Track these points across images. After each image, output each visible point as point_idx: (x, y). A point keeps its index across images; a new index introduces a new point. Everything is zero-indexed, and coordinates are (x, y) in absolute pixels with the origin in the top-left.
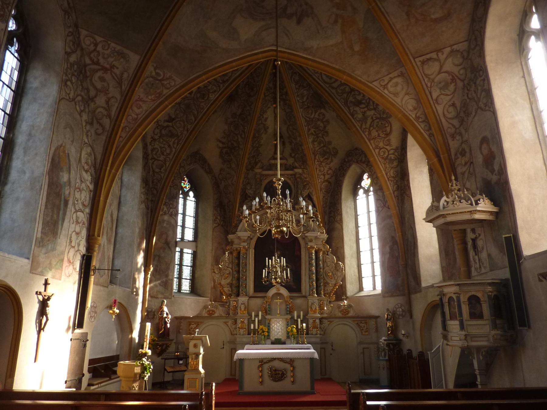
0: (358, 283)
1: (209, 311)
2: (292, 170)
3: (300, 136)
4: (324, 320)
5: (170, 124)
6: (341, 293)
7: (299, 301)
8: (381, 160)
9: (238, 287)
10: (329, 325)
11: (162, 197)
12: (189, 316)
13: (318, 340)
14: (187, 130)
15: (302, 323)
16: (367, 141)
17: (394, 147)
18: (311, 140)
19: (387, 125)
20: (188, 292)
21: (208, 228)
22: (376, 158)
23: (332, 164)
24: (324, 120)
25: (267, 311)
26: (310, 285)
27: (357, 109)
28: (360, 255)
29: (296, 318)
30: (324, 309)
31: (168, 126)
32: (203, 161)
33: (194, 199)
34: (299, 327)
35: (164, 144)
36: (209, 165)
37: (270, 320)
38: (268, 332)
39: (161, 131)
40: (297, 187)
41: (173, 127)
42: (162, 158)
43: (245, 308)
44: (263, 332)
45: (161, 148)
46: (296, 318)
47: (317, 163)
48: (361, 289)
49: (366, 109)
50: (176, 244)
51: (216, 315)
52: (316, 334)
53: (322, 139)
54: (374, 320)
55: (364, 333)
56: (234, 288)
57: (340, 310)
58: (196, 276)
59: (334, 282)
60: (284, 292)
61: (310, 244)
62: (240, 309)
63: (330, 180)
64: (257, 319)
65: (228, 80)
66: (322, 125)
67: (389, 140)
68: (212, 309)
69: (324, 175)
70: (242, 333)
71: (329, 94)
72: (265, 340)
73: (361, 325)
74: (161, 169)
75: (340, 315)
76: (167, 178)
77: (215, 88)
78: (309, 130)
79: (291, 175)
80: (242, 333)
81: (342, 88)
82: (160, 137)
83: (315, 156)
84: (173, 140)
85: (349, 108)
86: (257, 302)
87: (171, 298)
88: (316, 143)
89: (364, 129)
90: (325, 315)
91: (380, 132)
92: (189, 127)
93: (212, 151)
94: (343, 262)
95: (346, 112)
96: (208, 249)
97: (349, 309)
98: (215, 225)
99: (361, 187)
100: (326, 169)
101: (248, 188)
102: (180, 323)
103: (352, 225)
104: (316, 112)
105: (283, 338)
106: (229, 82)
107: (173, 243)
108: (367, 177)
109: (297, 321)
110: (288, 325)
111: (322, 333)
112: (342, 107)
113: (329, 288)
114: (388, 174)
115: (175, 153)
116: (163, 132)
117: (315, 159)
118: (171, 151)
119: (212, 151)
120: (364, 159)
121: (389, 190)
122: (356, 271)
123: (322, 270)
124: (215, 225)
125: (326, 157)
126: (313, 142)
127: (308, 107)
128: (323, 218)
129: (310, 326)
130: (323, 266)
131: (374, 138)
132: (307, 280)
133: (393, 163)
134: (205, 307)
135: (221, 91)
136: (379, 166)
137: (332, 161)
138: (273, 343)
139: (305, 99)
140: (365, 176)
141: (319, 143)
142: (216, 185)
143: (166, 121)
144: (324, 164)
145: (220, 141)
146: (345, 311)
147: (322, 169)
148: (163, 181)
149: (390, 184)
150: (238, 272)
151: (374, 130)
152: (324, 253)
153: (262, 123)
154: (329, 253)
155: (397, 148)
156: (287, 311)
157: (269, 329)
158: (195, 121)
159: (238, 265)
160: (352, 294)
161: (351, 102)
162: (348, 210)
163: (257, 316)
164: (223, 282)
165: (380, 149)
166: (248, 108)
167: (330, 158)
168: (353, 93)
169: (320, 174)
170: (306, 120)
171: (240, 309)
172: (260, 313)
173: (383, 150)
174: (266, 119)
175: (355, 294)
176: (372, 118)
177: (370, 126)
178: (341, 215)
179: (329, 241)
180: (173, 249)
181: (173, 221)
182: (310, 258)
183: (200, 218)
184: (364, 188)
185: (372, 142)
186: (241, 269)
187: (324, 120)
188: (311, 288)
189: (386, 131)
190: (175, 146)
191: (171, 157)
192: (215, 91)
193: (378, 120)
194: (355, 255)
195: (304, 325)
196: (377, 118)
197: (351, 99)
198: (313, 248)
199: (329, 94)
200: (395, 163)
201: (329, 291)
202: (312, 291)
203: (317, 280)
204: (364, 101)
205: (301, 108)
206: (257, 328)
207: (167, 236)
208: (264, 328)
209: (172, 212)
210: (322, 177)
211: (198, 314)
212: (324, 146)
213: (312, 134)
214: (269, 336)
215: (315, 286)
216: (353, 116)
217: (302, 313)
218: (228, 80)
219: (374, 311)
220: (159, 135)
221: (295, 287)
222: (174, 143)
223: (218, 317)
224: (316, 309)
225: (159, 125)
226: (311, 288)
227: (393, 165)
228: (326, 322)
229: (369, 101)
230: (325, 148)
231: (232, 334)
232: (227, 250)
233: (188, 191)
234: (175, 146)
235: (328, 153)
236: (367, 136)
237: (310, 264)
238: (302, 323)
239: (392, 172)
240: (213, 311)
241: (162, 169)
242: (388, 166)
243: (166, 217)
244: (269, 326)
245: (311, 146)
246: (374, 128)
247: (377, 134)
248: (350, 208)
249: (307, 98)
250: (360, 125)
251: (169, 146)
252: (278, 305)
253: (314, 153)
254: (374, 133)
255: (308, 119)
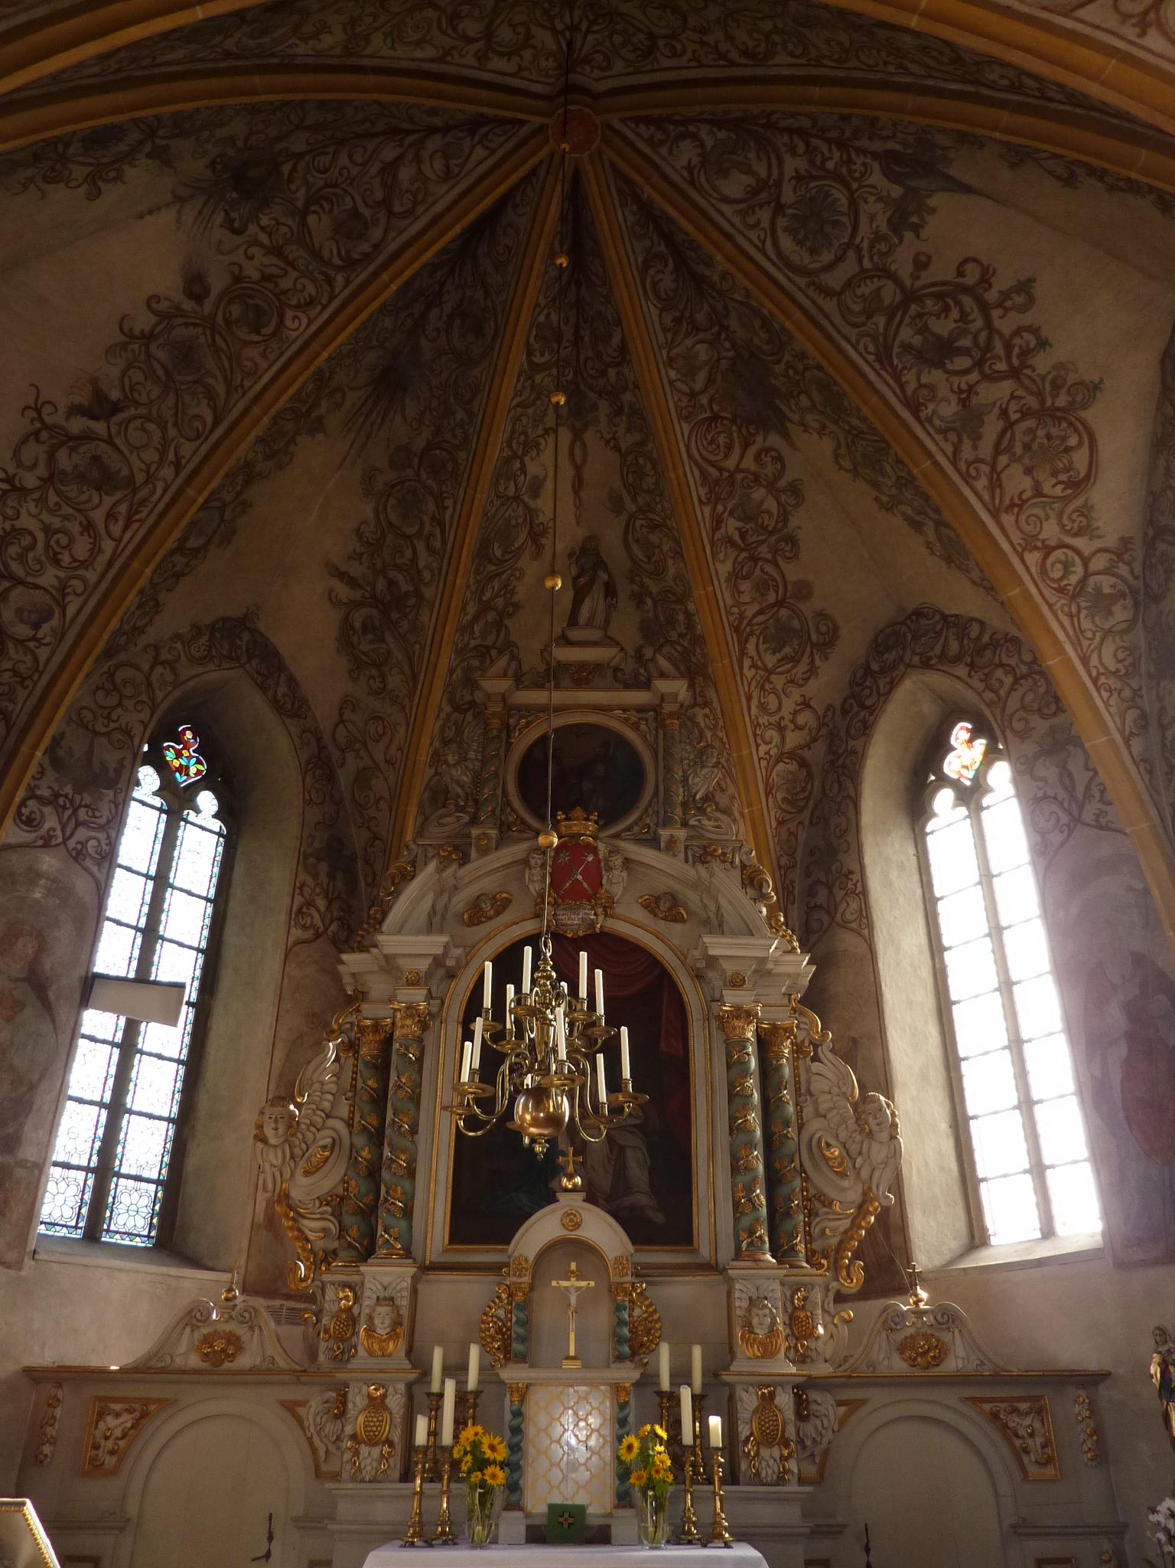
0: (959, 1209)
1: (207, 1340)
2: (647, 685)
3: (678, 553)
4: (814, 1395)
5: (99, 427)
6: (885, 1260)
7: (682, 1293)
8: (1052, 600)
9: (369, 1214)
10: (842, 1422)
11: (25, 749)
12: (95, 1362)
13: (791, 1515)
14: (178, 466)
15: (700, 1413)
16: (985, 516)
17: (1111, 540)
18: (724, 568)
19: (1073, 441)
20: (138, 1242)
21: (267, 940)
22: (1033, 590)
23: (813, 686)
24: (782, 483)
25: (513, 1339)
26: (736, 1205)
27: (936, 377)
28: (960, 1078)
29: (665, 1385)
30: (811, 1334)
31: (87, 436)
32: (268, 664)
33: (216, 825)
34: (687, 1438)
35: (65, 518)
36: (292, 682)
37: (523, 1393)
38: (513, 1466)
39: (51, 456)
40: (667, 751)
41: (111, 442)
42: (49, 578)
43: (397, 1323)
44: (481, 1464)
45: (47, 529)
46: (665, 1385)
47: (749, 674)
48: (976, 1236)
49: (975, 376)
50: (91, 988)
51: (245, 1361)
52: (780, 1480)
53: (771, 570)
54: (1083, 1394)
55: (1032, 1469)
56: (348, 1220)
57: (900, 1337)
58: (192, 1163)
59: (854, 1195)
60: (602, 1231)
61: (732, 999)
62: (371, 1331)
63: (806, 754)
64: (450, 1388)
65: (367, 257)
66: (771, 504)
67: (1086, 511)
68: (227, 1327)
69: (781, 729)
70: (368, 1473)
71: (806, 312)
72: (485, 1518)
73: (1014, 1421)
74: (37, 627)
75: (899, 1366)
76: (63, 665)
77: (311, 289)
78: (718, 522)
79: (641, 709)
80: (368, 1473)
81: (865, 290)
82: (47, 481)
83: (743, 643)
84: (108, 501)
85: (897, 377)
86: (458, 1298)
87: (18, 1265)
88: (745, 586)
89: (969, 464)
90: (822, 1369)
91: (1041, 475)
92: (187, 449)
93: (306, 626)
94: (889, 1095)
95: (889, 395)
96: (254, 1030)
97: (946, 1337)
98: (297, 933)
99: (944, 781)
100: (789, 705)
101: (451, 759)
102: (53, 1402)
103: (914, 940)
104: (745, 447)
105: (597, 1503)
106: (372, 268)
107: (70, 982)
108: (967, 736)
109: (674, 1399)
110: (622, 1422)
111: (811, 1470)
112: (867, 370)
113: (833, 1226)
114: (1094, 661)
115: (110, 564)
116: (64, 460)
117: (743, 653)
118: (95, 550)
119: (306, 626)
120: (954, 647)
121: (1106, 731)
122: (948, 1146)
123: (792, 1132)
124: (297, 933)
125: (787, 650)
126: (735, 577)
127: (714, 418)
128: (786, 890)
129: (744, 1431)
130: (799, 1113)
131: (1018, 505)
132: (723, 1178)
133: (1110, 613)
134: (194, 1316)
135: (336, 303)
136: (1041, 615)
137: (812, 671)
138: (537, 1536)
139: (701, 378)
140: (960, 733)
141: (761, 588)
142: (321, 766)
143: (76, 410)
144: (779, 681)
145: (342, 575)
146: (924, 1350)
147: (772, 702)
148: (46, 678)
149: (1107, 704)
150: (377, 1137)
151: (1016, 469)
152: (798, 1049)
153: (517, 498)
154: (825, 1052)
155: (1126, 542)
156: (620, 1340)
157: (515, 1448)
158: (217, 422)
159: (379, 1100)
160: (938, 1261)
161: (907, 348)
162: (894, 875)
163: (456, 1369)
164: (302, 1189)
165: (1048, 550)
166: (460, 415)
167: (806, 660)
168: (914, 309)
169: (764, 720)
170: (705, 477)
171: (371, 1331)
172: (474, 1352)
173: (1058, 554)
174: (536, 489)
175: (953, 1261)
176: (1004, 413)
177: (997, 451)
178: (864, 893)
179: (815, 998)
180: (63, 1014)
181: (82, 885)
182: (735, 1066)
183: (234, 907)
184: (956, 785)
185: (1007, 519)
186: (389, 1115)
187: (782, 483)
188: (745, 1222)
189: (1067, 470)
190: (116, 529)
191: (91, 576)
192: (311, 302)
193: (1031, 423)
194: (938, 1076)
195: (715, 1422)
196: (1026, 413)
197: (906, 335)
198: (749, 1015)
199: (806, 312)
200: (1121, 614)
201: (835, 1241)
202: (751, 1232)
203: (774, 1180)
204: (965, 342)
205: (687, 418)
206: (447, 1438)
207: (42, 949)
208: (486, 1441)
209: (84, 844)
210: (772, 734)
211: (154, 1354)
212: (780, 603)
213: (730, 541)
214: (514, 1487)
215: (764, 1211)
216: (915, 409)
217: (697, 1352)
218: (367, 257)
219: (1071, 1347)
220: (42, 470)
221: (659, 1218)
222: (110, 516)
223: (253, 1371)
224: (772, 1330)
225: (45, 426)
226: (745, 1222)
227: (1112, 621)
228: (824, 1403)
229: (989, 339)
230: (783, 612)
231: (318, 1474)
232: (332, 1034)
233: (193, 789)
234: (116, 529)
235: (796, 635)
236: (986, 497)
237: (736, 1096)
238: (700, 1413)
239: (1108, 649)
240: (233, 1340)
241: (46, 627)
242: (1086, 624)
243: (49, 862)
244: (517, 1431)
245: (725, 596)
246: (1014, 459)
247: (1027, 483)
248: (902, 867)
249: (710, 381)
250: (949, 450)
251: (89, 527)
252: (571, 1308)
253: (737, 630)
254: (1017, 482)
255: (715, 473)
